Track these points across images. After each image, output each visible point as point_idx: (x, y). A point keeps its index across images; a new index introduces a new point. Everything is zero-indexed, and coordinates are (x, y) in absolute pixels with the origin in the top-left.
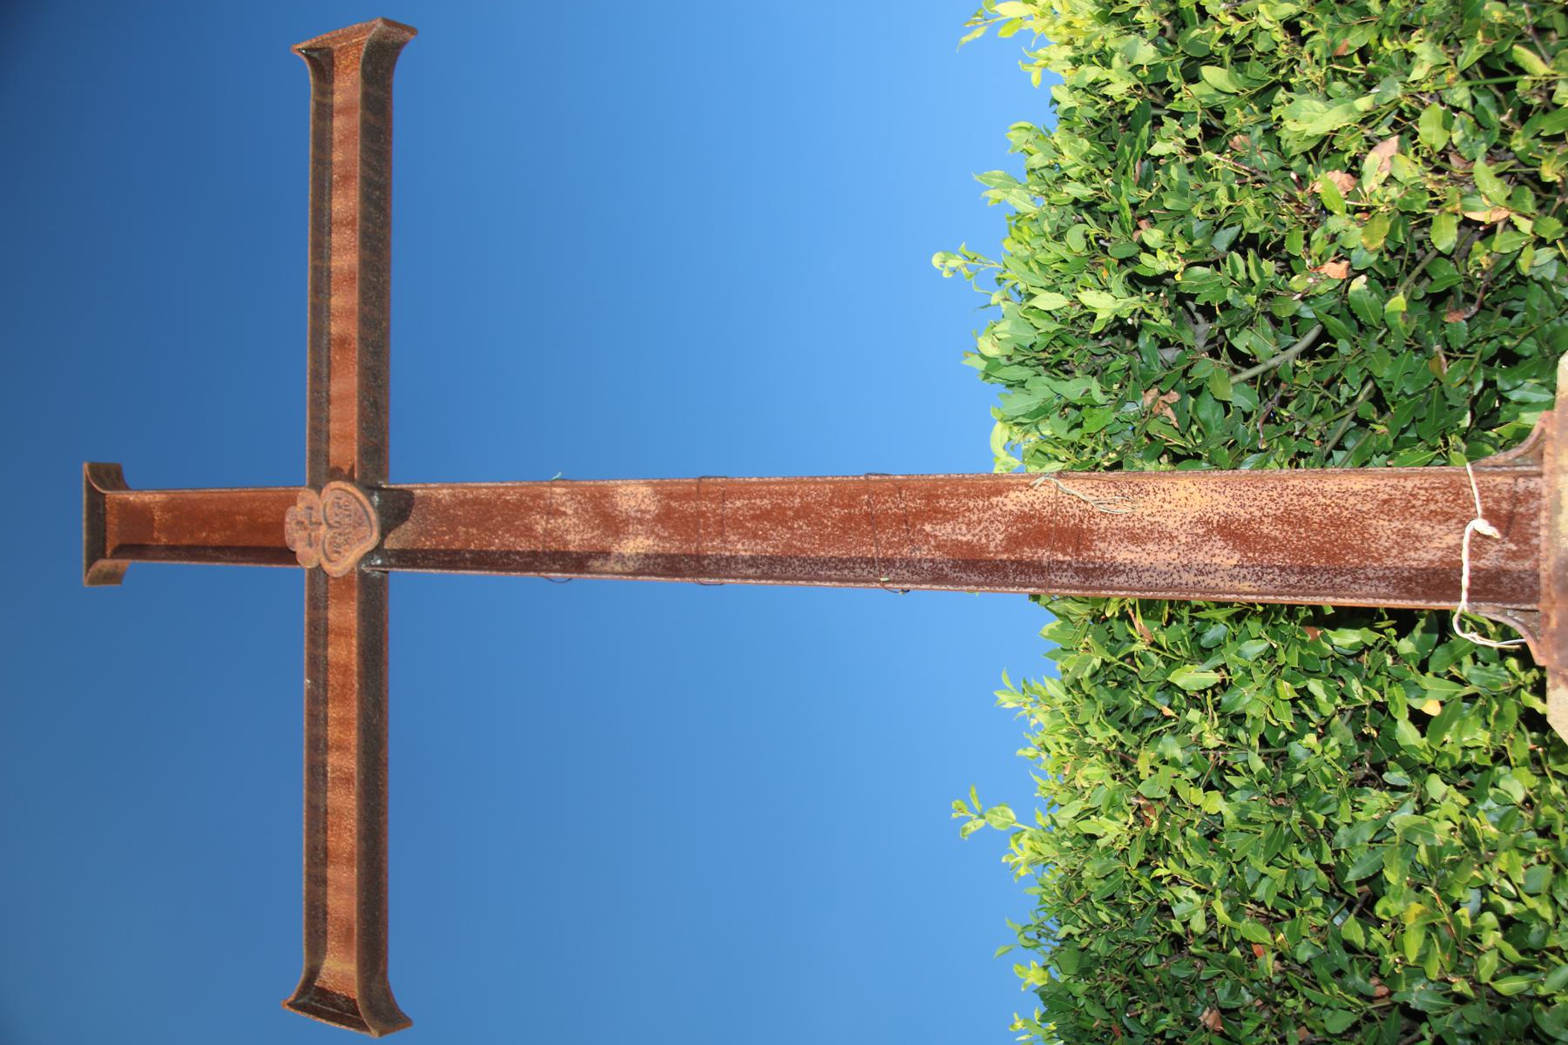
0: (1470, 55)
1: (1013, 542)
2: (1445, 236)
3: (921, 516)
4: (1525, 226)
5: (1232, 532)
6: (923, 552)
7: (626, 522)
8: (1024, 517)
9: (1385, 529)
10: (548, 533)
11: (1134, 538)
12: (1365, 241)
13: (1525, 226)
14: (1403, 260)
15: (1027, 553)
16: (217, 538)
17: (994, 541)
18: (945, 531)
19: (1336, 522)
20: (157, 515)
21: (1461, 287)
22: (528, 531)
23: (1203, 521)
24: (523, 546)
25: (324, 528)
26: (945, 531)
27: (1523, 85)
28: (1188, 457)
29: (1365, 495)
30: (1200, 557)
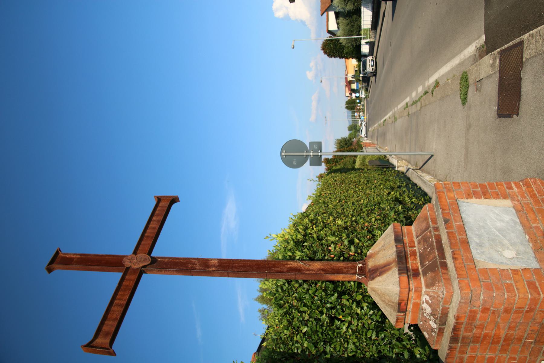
3: (272, 267)
7: (211, 266)
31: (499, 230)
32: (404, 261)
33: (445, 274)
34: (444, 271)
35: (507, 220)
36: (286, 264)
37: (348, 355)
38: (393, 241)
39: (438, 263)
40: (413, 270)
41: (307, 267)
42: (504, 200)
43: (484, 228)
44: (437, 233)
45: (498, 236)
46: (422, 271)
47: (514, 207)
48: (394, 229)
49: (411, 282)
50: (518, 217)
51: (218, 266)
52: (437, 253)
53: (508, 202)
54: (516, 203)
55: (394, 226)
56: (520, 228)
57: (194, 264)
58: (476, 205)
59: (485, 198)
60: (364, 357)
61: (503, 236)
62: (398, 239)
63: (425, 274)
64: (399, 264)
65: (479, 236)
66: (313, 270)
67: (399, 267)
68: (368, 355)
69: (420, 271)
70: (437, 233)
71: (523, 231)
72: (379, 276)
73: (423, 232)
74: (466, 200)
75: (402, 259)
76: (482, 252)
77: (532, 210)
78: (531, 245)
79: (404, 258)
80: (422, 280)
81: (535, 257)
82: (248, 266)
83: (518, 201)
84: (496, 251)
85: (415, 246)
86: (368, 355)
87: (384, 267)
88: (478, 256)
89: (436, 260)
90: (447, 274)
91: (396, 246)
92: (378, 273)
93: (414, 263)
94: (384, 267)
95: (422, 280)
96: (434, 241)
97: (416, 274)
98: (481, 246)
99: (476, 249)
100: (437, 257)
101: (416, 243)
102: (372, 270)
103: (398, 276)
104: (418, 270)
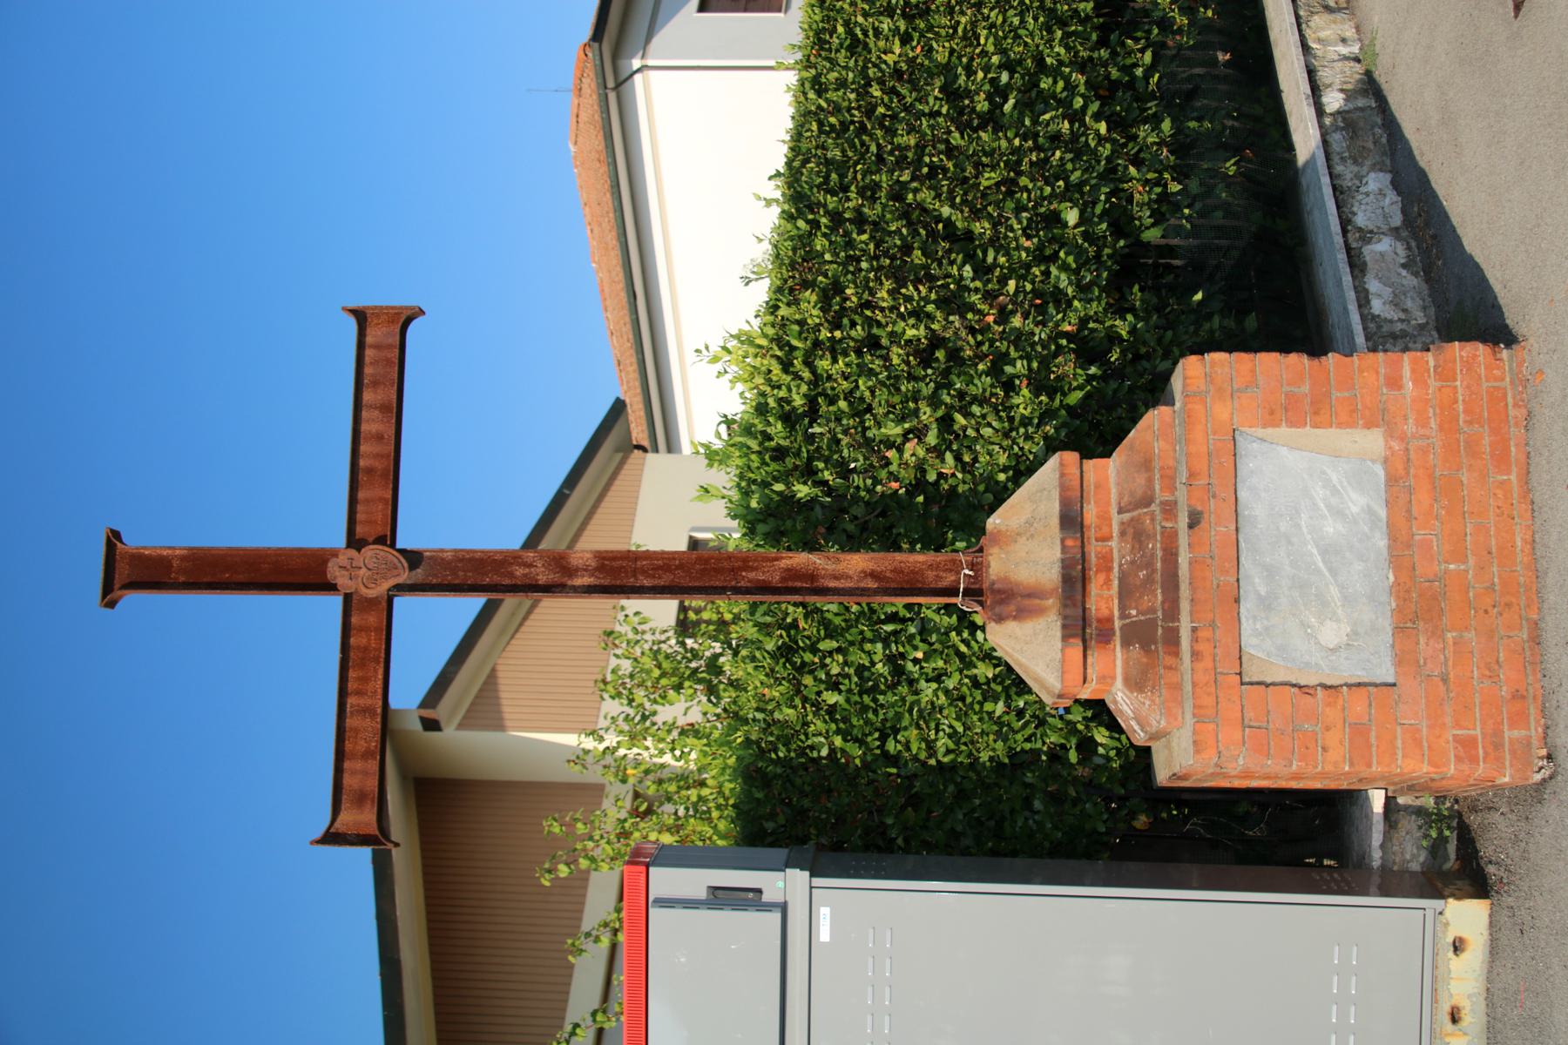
0: (940, 413)
1: (783, 579)
2: (932, 477)
3: (741, 569)
4: (960, 476)
5: (873, 575)
6: (742, 584)
7: (577, 570)
8: (788, 570)
9: (931, 574)
10: (525, 575)
11: (836, 578)
12: (908, 475)
13: (960, 476)
14: (919, 485)
15: (790, 584)
16: (241, 578)
17: (775, 579)
18: (752, 575)
19: (913, 572)
20: (175, 563)
21: (606, 696)
22: (511, 575)
23: (863, 571)
24: (507, 581)
25: (364, 570)
26: (752, 575)
27: (956, 427)
28: (1394, 337)
29: (923, 563)
30: (862, 585)
31: (1324, 552)
32: (1079, 597)
33: (1170, 668)
34: (1169, 660)
35: (1355, 510)
36: (776, 559)
37: (938, 762)
38: (1055, 521)
39: (1160, 631)
40: (1099, 621)
41: (831, 567)
42: (1366, 432)
43: (1290, 543)
44: (1169, 525)
45: (1318, 571)
46: (1121, 629)
47: (1386, 461)
48: (1062, 475)
49: (1090, 660)
50: (1387, 502)
51: (596, 569)
52: (1160, 597)
53: (1372, 441)
54: (1396, 445)
55: (1061, 464)
56: (1382, 542)
57: (530, 566)
58: (1284, 451)
59: (1315, 426)
60: (974, 764)
61: (1330, 570)
62: (1071, 520)
63: (1126, 643)
64: (1065, 606)
65: (1271, 572)
66: (848, 577)
67: (1065, 618)
68: (984, 757)
69: (1117, 624)
70: (1169, 525)
71: (1385, 552)
72: (1015, 618)
73: (1136, 507)
74: (1260, 432)
75: (1075, 579)
76: (1267, 629)
77: (1431, 476)
78: (1394, 605)
79: (1079, 586)
80: (1119, 654)
81: (1393, 646)
82: (677, 568)
83: (1403, 438)
84: (1302, 624)
85: (1110, 538)
86: (984, 757)
87: (1029, 596)
88: (1254, 641)
89: (1155, 620)
90: (1176, 669)
91: (1063, 541)
92: (1011, 608)
93: (1103, 598)
94: (1029, 596)
95: (1119, 654)
96: (1159, 553)
97: (1105, 636)
98: (1269, 608)
99: (1255, 618)
100: (1160, 614)
101: (1115, 533)
102: (999, 591)
103: (1059, 644)
104: (1110, 620)
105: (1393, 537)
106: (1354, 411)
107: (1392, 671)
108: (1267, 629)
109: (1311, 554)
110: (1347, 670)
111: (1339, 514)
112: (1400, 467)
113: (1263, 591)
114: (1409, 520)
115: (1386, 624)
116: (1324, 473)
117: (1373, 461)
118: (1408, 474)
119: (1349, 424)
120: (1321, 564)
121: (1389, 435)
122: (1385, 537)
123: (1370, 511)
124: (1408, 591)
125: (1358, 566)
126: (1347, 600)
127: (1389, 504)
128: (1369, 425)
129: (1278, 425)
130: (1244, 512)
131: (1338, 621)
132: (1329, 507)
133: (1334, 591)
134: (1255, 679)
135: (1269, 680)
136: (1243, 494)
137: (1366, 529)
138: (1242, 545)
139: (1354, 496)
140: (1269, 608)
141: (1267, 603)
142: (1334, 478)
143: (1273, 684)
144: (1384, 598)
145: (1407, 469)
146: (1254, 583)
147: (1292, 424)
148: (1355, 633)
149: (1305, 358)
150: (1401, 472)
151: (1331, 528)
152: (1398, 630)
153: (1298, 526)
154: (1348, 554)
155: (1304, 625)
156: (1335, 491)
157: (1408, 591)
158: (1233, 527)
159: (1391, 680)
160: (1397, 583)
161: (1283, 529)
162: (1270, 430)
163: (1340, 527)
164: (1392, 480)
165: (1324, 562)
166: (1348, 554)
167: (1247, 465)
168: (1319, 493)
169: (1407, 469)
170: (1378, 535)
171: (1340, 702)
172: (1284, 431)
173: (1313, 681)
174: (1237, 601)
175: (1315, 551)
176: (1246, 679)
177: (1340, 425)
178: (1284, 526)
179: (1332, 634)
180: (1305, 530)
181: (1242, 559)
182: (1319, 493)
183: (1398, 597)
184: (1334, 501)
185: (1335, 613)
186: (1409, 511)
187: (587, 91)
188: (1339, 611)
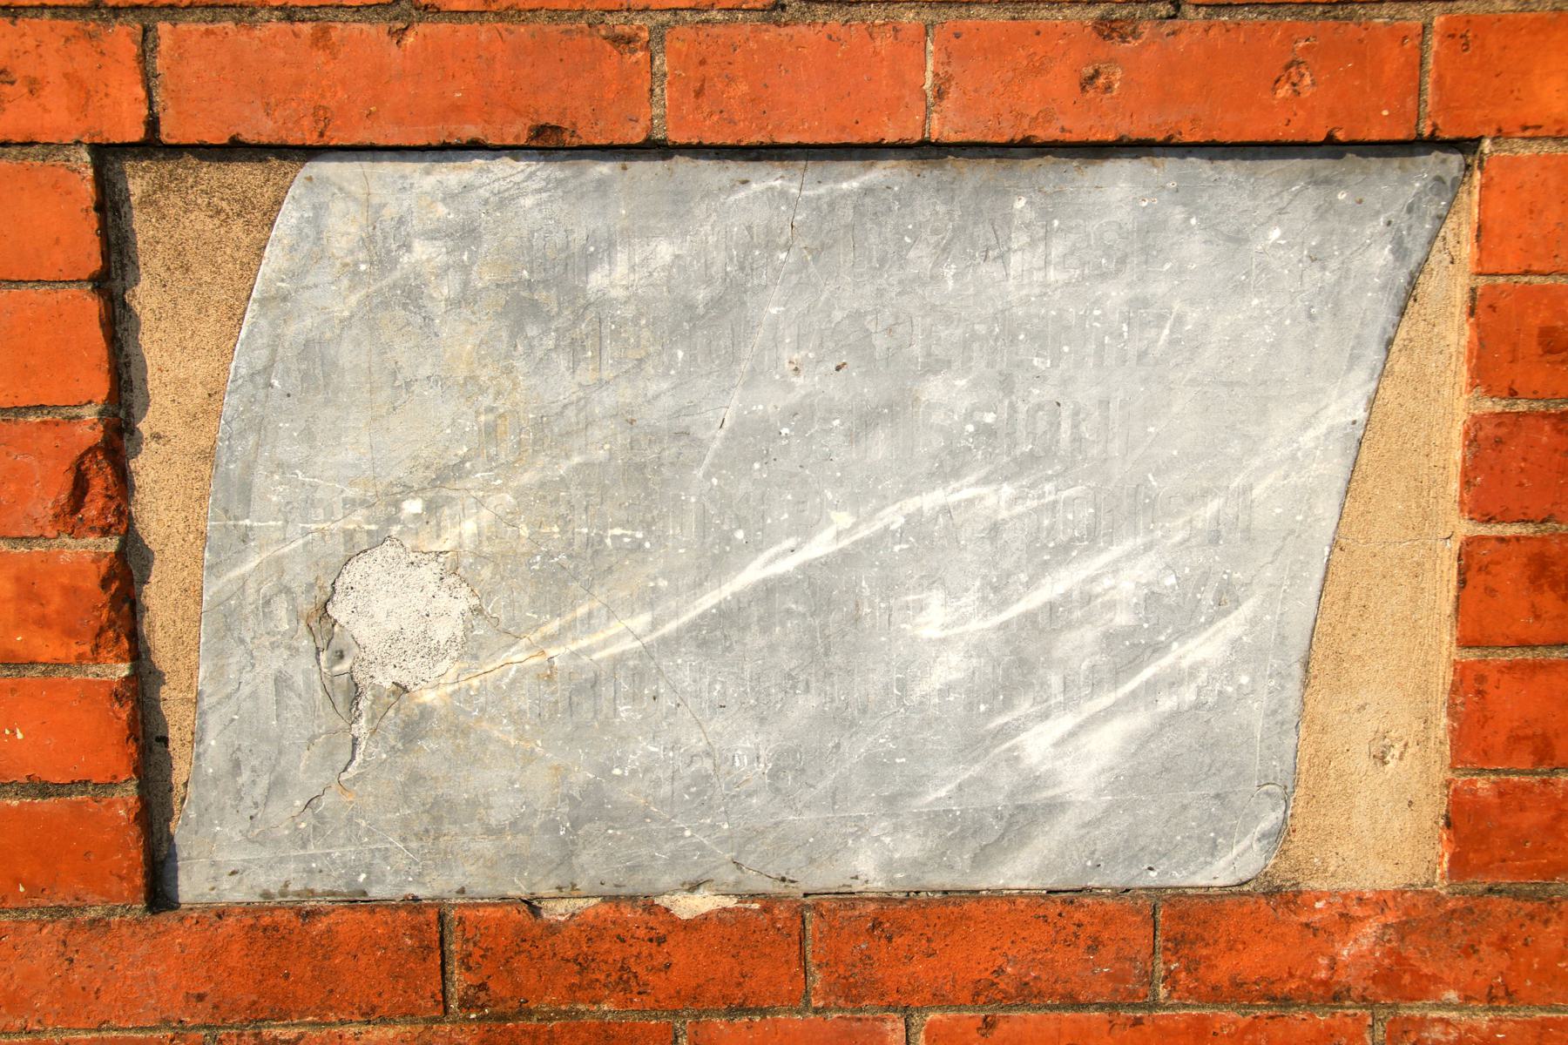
31: (817, 589)
35: (1036, 745)
42: (1433, 808)
43: (865, 422)
45: (716, 564)
47: (1277, 896)
50: (1072, 897)
53: (1383, 831)
54: (1359, 946)
56: (870, 864)
58: (1345, 405)
59: (1471, 563)
61: (726, 617)
65: (706, 320)
74: (1450, 285)
76: (411, 295)
78: (557, 911)
81: (357, 902)
83: (1395, 979)
88: (344, 230)
99: (466, 234)
105: (898, 918)
106: (1544, 752)
107: (235, 893)
108: (411, 295)
109: (805, 530)
110: (231, 697)
111: (1016, 667)
112: (1252, 961)
113: (610, 279)
114: (981, 993)
115: (465, 872)
116: (1227, 599)
117: (1281, 836)
118: (1216, 996)
119: (1473, 734)
120: (753, 573)
121: (1414, 917)
122: (901, 881)
123: (1027, 814)
124: (625, 980)
125: (748, 749)
126: (579, 694)
127: (1061, 906)
128: (1464, 823)
129: (1483, 374)
130: (1024, 194)
131: (470, 649)
132: (1054, 616)
133: (621, 634)
134: (143, 226)
135: (145, 297)
136: (1119, 188)
137: (937, 794)
138: (852, 180)
139: (1107, 742)
140: (521, 308)
141: (540, 300)
142: (1203, 649)
143: (117, 324)
144: (598, 867)
145: (1236, 992)
146: (653, 238)
147: (1486, 447)
148: (413, 729)
149: (164, 692)
150: (1223, 969)
151: (944, 632)
152: (431, 928)
153: (949, 467)
154: (807, 704)
155: (441, 482)
156: (1128, 652)
157: (625, 980)
158: (939, 129)
159: (192, 886)
160: (665, 929)
161: (933, 389)
162: (1456, 335)
163: (949, 668)
164: (1184, 920)
165: (768, 590)
166: (807, 704)
167: (1273, 214)
168: (1123, 574)
169: (1236, 992)
170: (910, 846)
171: (47, 646)
172: (1450, 407)
173: (159, 511)
174: (547, 143)
175: (821, 546)
176: (138, 182)
177: (1469, 686)
178: (949, 396)
179: (399, 611)
180: (931, 500)
181: (769, 179)
182: (1123, 574)
183: (591, 930)
184: (1079, 645)
185: (510, 634)
186: (1025, 995)
187: (1103, 778)
188: (518, 655)
